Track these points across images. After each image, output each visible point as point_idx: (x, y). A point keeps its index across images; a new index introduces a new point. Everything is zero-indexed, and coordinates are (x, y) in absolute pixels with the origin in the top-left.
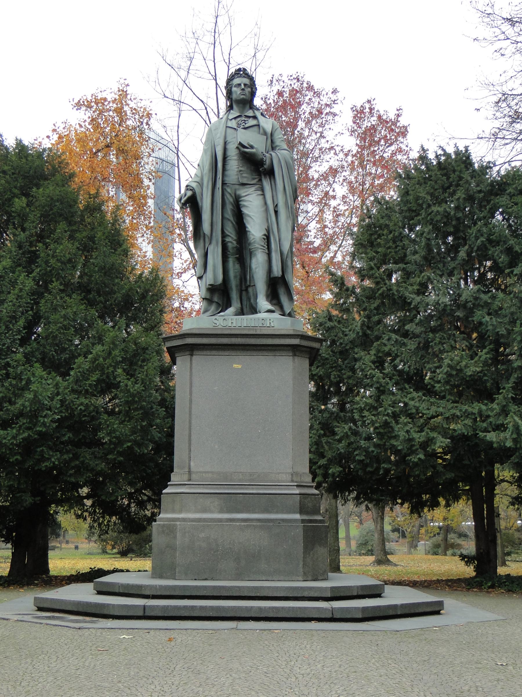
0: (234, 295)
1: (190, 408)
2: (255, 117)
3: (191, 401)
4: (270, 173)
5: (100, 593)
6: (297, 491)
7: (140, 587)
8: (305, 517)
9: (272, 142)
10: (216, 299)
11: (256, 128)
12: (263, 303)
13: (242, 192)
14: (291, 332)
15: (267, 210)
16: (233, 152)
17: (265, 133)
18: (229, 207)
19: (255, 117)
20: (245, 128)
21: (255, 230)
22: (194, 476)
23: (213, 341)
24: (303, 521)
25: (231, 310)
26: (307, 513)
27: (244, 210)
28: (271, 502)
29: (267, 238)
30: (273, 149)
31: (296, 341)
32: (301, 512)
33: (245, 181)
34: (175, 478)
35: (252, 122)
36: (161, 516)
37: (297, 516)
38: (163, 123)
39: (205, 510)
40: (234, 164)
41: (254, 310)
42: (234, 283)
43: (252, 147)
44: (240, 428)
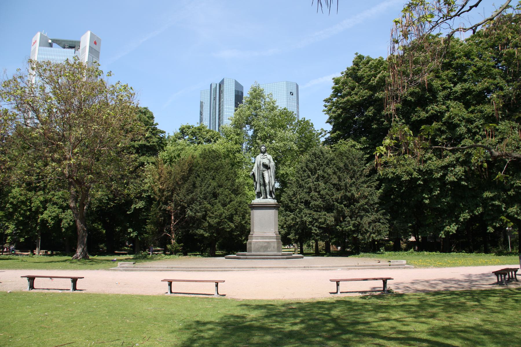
4: (270, 168)
12: (268, 196)
21: (267, 181)
25: (262, 197)
29: (269, 182)
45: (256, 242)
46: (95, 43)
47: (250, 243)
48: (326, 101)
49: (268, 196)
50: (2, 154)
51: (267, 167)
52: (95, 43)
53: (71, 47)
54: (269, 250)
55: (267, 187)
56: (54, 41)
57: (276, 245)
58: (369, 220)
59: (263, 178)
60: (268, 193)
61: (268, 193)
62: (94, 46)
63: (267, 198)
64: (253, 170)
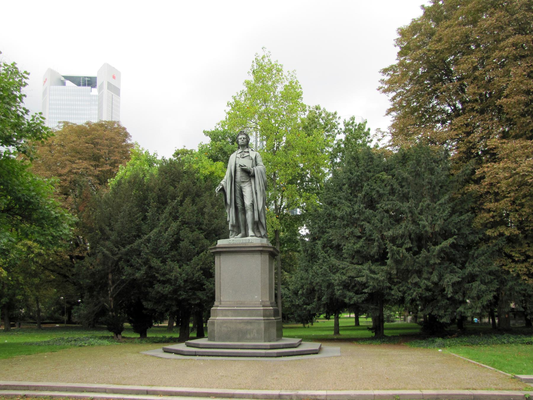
0: (242, 228)
1: (220, 276)
2: (248, 152)
3: (220, 274)
4: (254, 176)
5: (188, 346)
6: (262, 308)
7: (182, 351)
8: (266, 318)
9: (256, 162)
10: (235, 230)
11: (248, 157)
12: (251, 233)
13: (243, 185)
14: (260, 245)
15: (252, 192)
16: (238, 169)
17: (252, 159)
18: (238, 192)
19: (248, 152)
20: (243, 158)
21: (248, 202)
22: (222, 303)
23: (227, 250)
24: (264, 320)
25: (240, 235)
26: (267, 316)
27: (244, 193)
28: (251, 312)
29: (253, 205)
30: (256, 165)
31: (261, 249)
32: (264, 316)
33: (243, 180)
34: (216, 303)
35: (246, 154)
36: (211, 318)
37: (262, 318)
38: (372, 126)
39: (226, 316)
40: (239, 173)
41: (246, 235)
42: (241, 223)
43: (245, 166)
44: (241, 283)
45: (224, 322)
46: (114, 77)
47: (213, 323)
48: (385, 71)
49: (251, 233)
50: (530, 296)
51: (249, 174)
52: (114, 77)
53: (89, 85)
54: (248, 336)
55: (249, 214)
56: (67, 78)
57: (262, 326)
58: (456, 279)
59: (242, 196)
60: (250, 226)
61: (250, 226)
62: (113, 82)
63: (246, 235)
64: (222, 182)
